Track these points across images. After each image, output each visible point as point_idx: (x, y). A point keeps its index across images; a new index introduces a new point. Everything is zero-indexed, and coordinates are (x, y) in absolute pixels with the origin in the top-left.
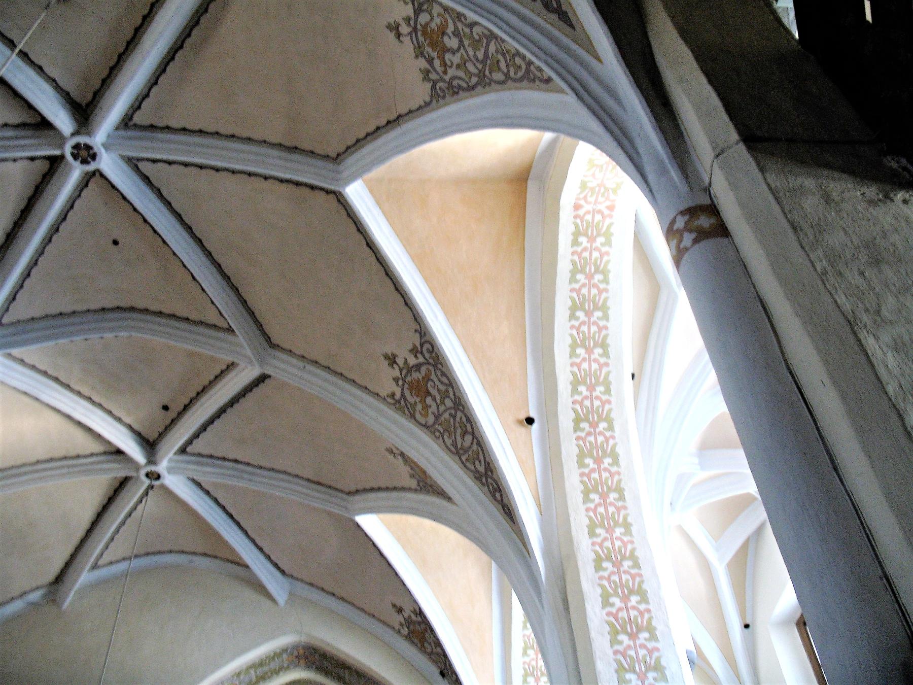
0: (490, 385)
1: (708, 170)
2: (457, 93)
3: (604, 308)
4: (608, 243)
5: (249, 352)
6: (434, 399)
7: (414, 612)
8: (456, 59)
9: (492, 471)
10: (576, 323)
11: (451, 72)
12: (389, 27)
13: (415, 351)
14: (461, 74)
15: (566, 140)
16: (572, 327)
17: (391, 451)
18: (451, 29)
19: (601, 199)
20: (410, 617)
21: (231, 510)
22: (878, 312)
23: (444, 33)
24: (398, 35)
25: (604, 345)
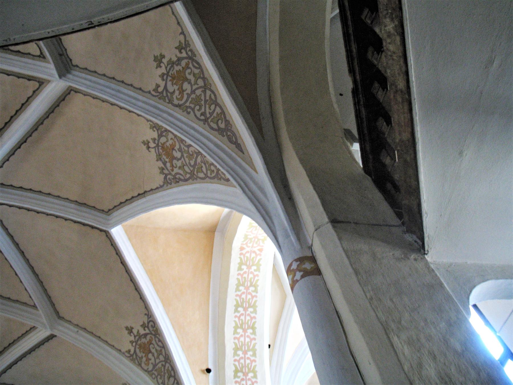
0: (186, 349)
1: (311, 235)
2: (178, 182)
3: (254, 306)
4: (258, 270)
5: (44, 320)
8: (179, 164)
10: (238, 315)
11: (176, 170)
12: (144, 143)
13: (144, 326)
14: (181, 172)
15: (236, 214)
16: (236, 317)
18: (177, 147)
19: (255, 245)
22: (400, 322)
23: (173, 149)
24: (148, 148)
25: (253, 328)
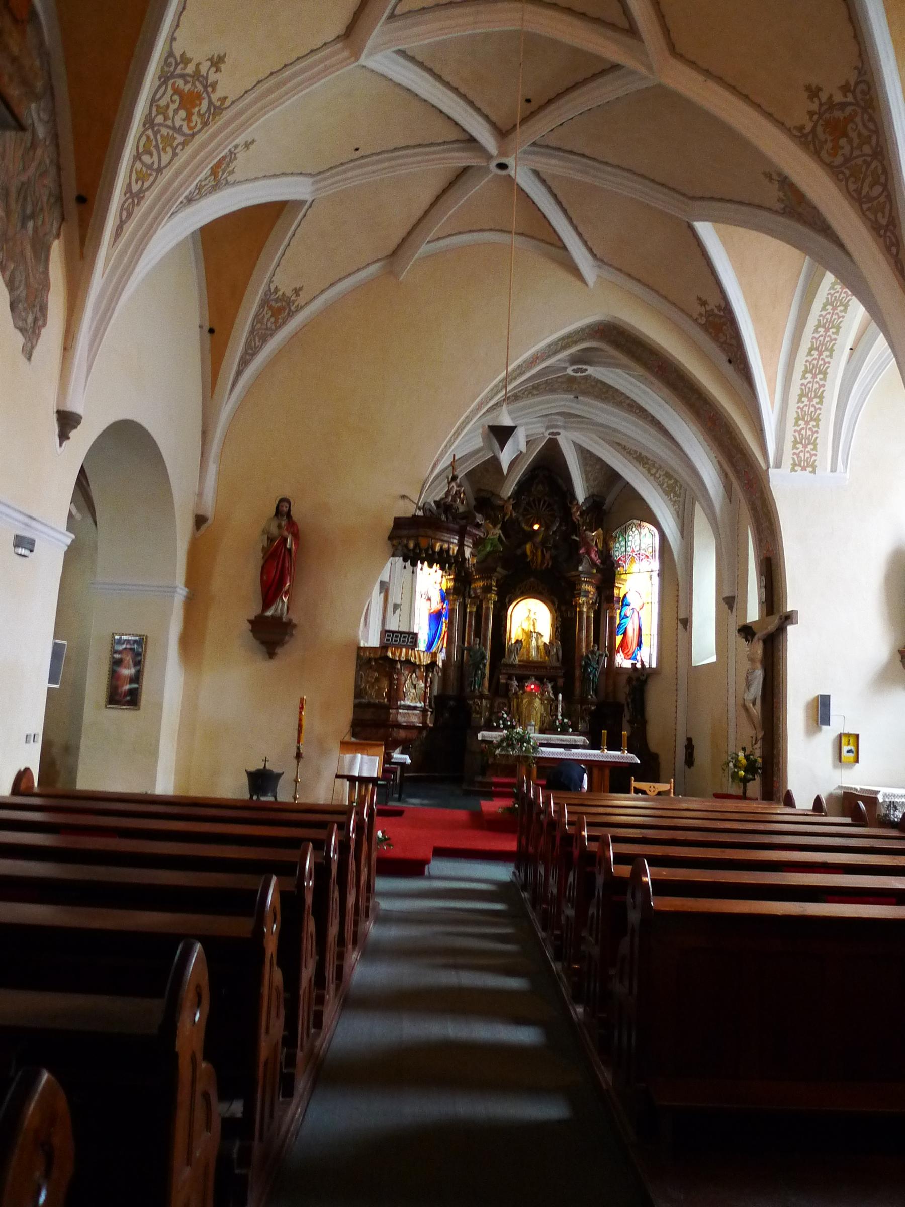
6: (850, 141)
7: (719, 308)
9: (895, 227)
10: (798, 429)
17: (769, 176)
20: (713, 310)
21: (555, 191)
